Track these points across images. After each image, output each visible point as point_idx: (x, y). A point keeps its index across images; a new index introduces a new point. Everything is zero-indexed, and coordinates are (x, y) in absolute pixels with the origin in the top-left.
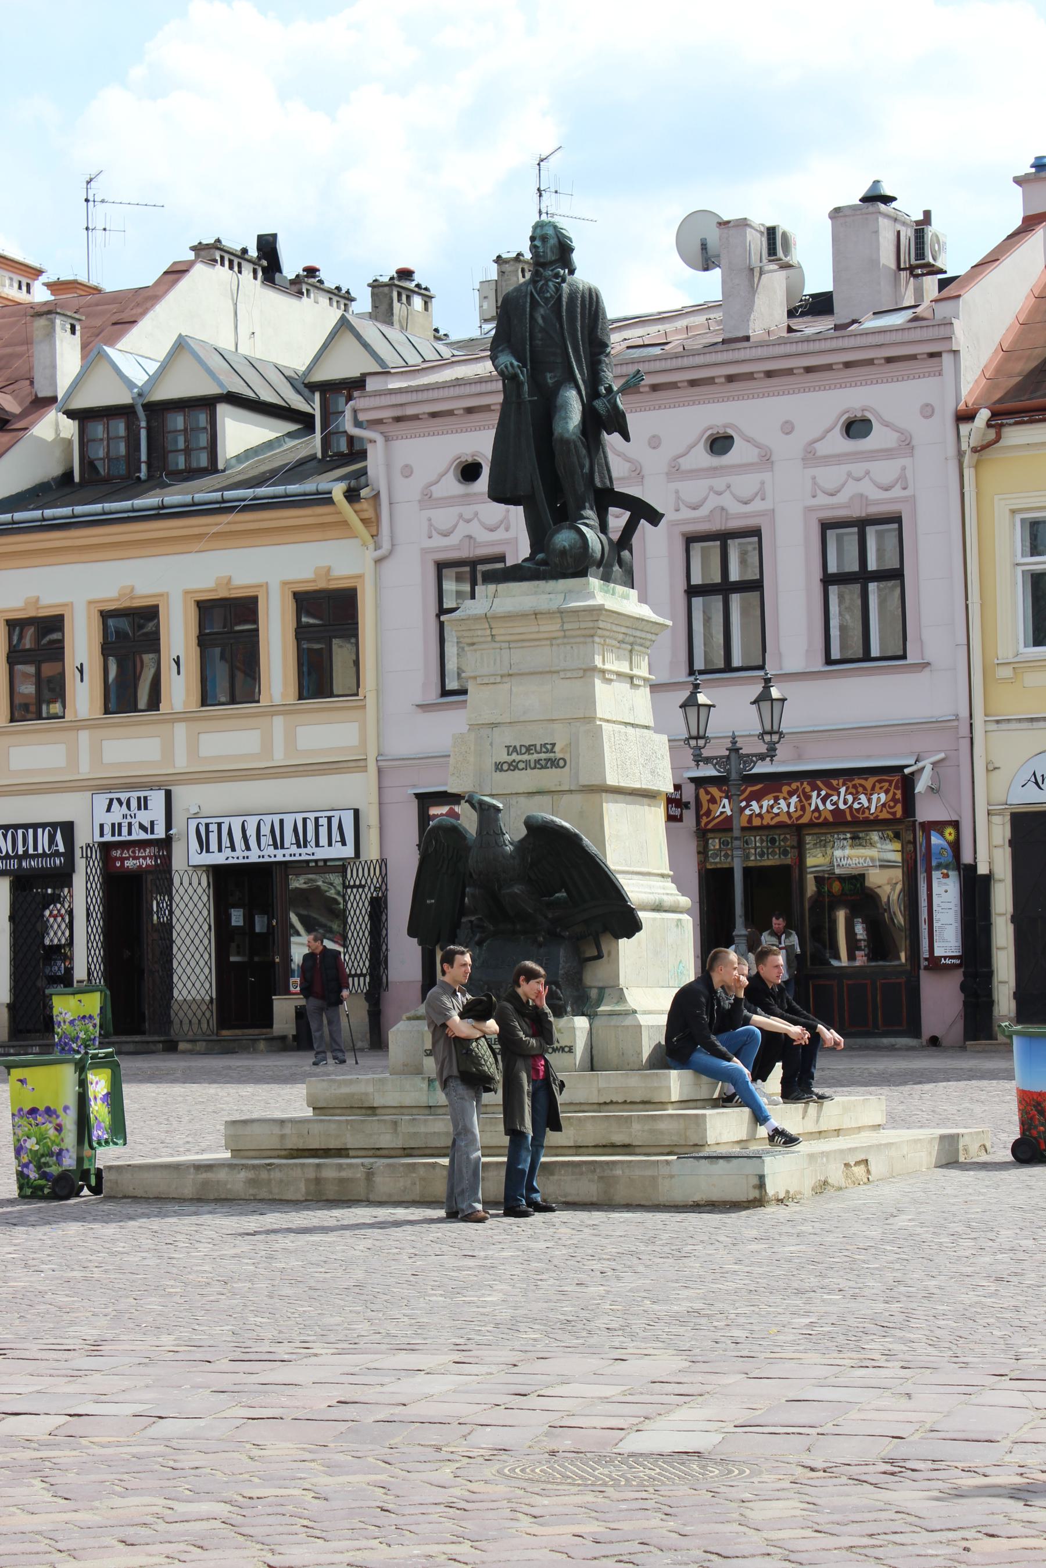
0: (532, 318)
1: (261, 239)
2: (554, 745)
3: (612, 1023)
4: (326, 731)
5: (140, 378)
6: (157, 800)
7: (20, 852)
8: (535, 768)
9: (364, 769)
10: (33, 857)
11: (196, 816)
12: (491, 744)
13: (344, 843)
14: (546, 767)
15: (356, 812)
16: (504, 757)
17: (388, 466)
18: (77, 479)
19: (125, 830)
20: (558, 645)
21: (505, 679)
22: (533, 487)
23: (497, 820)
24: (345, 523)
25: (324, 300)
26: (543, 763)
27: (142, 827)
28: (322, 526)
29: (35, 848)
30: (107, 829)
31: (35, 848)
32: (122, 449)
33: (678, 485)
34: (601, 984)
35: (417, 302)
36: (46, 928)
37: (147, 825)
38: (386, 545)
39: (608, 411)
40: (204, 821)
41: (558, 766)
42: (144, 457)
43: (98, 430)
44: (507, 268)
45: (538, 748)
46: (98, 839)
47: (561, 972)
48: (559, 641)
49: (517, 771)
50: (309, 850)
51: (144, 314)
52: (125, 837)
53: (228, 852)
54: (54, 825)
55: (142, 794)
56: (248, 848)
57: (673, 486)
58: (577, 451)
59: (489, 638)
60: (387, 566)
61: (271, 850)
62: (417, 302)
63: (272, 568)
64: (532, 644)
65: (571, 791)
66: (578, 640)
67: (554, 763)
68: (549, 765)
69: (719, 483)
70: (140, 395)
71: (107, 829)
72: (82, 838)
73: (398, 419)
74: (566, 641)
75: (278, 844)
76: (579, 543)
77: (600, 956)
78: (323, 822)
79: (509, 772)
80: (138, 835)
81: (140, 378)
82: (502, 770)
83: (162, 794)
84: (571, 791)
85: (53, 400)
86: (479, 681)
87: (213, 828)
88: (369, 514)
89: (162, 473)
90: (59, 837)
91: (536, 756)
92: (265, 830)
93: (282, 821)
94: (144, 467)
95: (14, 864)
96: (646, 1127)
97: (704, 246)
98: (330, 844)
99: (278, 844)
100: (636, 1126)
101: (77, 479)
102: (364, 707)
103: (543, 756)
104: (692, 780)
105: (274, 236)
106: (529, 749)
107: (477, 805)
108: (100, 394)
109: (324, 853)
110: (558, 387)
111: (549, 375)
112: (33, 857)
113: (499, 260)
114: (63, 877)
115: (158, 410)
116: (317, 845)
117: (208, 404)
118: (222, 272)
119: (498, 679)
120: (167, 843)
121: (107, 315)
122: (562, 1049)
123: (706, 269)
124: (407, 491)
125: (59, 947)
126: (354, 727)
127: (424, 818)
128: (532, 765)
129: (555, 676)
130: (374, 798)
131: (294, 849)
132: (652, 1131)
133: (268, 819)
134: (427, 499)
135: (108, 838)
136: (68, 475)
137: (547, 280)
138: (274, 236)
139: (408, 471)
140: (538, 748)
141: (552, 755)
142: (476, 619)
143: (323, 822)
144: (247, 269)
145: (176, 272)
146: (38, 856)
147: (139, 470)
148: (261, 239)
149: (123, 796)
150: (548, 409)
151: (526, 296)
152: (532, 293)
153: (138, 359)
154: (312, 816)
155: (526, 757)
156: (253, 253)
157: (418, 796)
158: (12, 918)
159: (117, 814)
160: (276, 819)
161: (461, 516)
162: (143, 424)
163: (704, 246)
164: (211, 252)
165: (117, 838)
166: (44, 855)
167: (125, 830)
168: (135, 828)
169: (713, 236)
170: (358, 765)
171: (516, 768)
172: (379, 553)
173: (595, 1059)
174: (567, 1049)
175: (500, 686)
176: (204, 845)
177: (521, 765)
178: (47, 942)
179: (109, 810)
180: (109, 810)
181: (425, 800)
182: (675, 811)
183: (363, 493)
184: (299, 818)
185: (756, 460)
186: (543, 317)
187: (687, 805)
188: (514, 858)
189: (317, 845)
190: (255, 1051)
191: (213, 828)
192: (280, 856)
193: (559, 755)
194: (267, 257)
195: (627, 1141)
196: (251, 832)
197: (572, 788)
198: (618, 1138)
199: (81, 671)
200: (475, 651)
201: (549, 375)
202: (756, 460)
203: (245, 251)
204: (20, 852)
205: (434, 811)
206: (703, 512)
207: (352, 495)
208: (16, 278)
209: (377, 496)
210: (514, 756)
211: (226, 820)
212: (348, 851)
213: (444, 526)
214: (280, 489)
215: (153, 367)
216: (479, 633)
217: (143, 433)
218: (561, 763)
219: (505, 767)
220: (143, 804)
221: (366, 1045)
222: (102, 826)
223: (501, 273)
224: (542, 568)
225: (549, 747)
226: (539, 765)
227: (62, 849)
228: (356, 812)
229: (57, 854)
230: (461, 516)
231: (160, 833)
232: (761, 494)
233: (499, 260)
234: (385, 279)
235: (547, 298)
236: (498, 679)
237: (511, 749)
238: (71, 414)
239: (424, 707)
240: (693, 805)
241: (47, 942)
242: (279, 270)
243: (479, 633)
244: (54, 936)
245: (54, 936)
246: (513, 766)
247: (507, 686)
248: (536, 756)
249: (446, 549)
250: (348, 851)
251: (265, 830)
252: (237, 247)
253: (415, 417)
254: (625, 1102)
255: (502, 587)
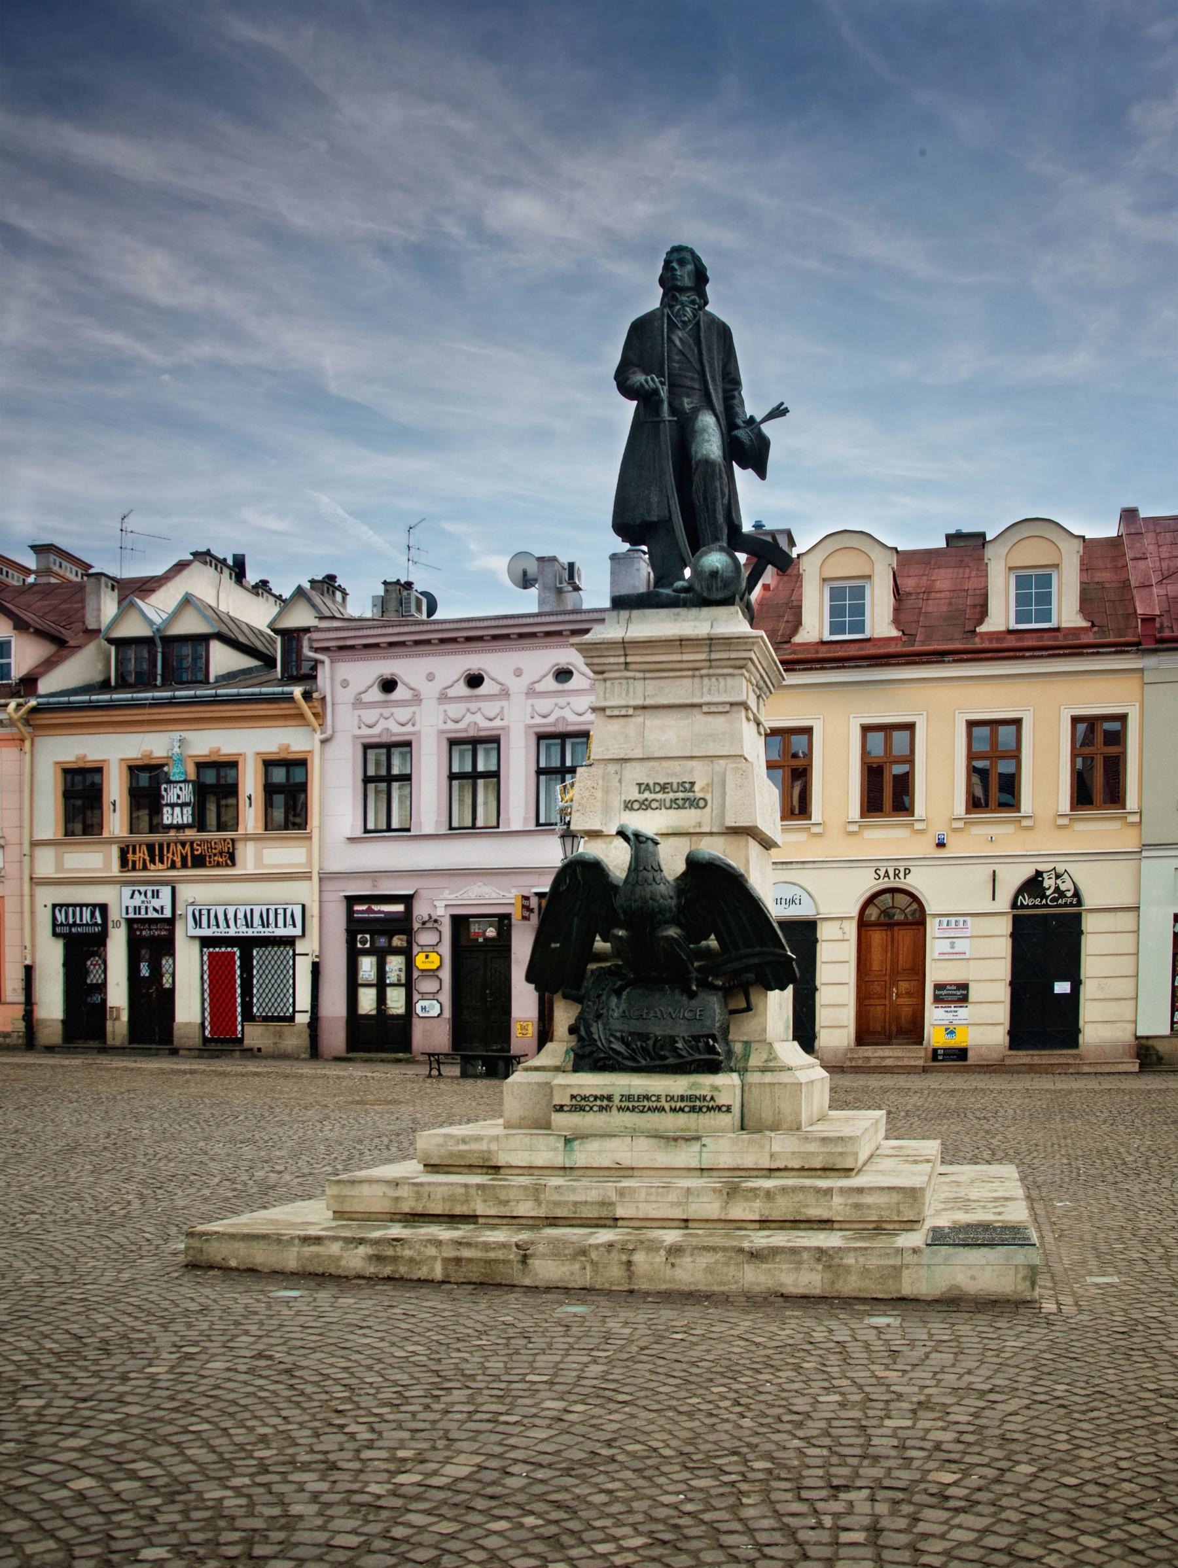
0: (670, 340)
1: (235, 556)
2: (692, 784)
3: (767, 1081)
4: (284, 854)
5: (158, 620)
6: (166, 892)
7: (71, 921)
8: (671, 808)
9: (310, 878)
10: (79, 925)
11: (192, 904)
12: (620, 781)
13: (294, 925)
14: (684, 808)
15: (304, 906)
16: (634, 794)
17: (332, 679)
18: (113, 683)
19: (143, 911)
20: (702, 676)
21: (638, 712)
22: (669, 511)
23: (655, 854)
24: (301, 716)
25: (272, 599)
26: (680, 802)
27: (155, 909)
28: (285, 717)
29: (81, 919)
30: (131, 910)
31: (81, 919)
32: (145, 666)
33: (533, 701)
34: (745, 1039)
35: (339, 595)
36: (87, 973)
37: (158, 908)
38: (329, 732)
39: (751, 440)
40: (198, 908)
41: (698, 807)
42: (159, 671)
43: (131, 654)
44: (390, 588)
45: (675, 786)
46: (124, 915)
47: (717, 1025)
48: (703, 672)
49: (649, 811)
50: (270, 929)
51: (160, 586)
52: (143, 915)
53: (214, 929)
54: (94, 906)
55: (155, 888)
56: (228, 926)
57: (530, 702)
58: (721, 477)
59: (622, 667)
60: (328, 746)
61: (244, 929)
62: (339, 595)
63: (249, 744)
64: (671, 674)
65: (711, 834)
66: (726, 671)
67: (694, 803)
68: (687, 805)
69: (562, 701)
70: (158, 630)
71: (131, 910)
72: (114, 914)
73: (341, 648)
74: (711, 671)
75: (249, 924)
76: (731, 567)
77: (749, 1009)
78: (281, 911)
79: (641, 811)
80: (152, 915)
81: (158, 621)
82: (632, 809)
83: (169, 889)
84: (711, 834)
85: (99, 631)
86: (608, 712)
87: (205, 912)
88: (319, 710)
89: (172, 677)
90: (97, 914)
91: (672, 795)
92: (240, 915)
93: (252, 910)
94: (159, 678)
95: (66, 930)
96: (850, 1201)
97: (525, 573)
98: (285, 926)
99: (249, 924)
100: (837, 1200)
101: (113, 683)
102: (311, 838)
103: (680, 795)
104: (537, 894)
105: (244, 556)
106: (664, 788)
107: (631, 837)
108: (133, 628)
109: (281, 932)
110: (696, 411)
111: (686, 400)
112: (79, 925)
113: (385, 583)
114: (99, 940)
115: (171, 641)
116: (276, 926)
117: (204, 639)
118: (210, 571)
119: (631, 712)
120: (171, 922)
121: (134, 590)
122: (719, 1108)
123: (525, 588)
124: (345, 696)
125: (97, 985)
126: (304, 850)
127: (350, 912)
128: (668, 805)
129: (696, 710)
130: (316, 897)
131: (260, 928)
132: (857, 1206)
133: (242, 908)
134: (358, 703)
135: (131, 915)
136: (108, 680)
137: (683, 305)
138: (244, 556)
139: (345, 684)
140: (675, 786)
141: (691, 794)
142: (610, 644)
143: (281, 911)
144: (226, 572)
145: (181, 566)
146: (83, 925)
147: (156, 680)
148: (235, 556)
149: (142, 889)
150: (685, 432)
151: (662, 319)
152: (668, 316)
153: (158, 608)
154: (273, 907)
155: (660, 796)
156: (230, 562)
157: (347, 897)
158: (65, 965)
159: (138, 900)
160: (248, 908)
161: (381, 715)
162: (160, 650)
163: (525, 573)
164: (204, 557)
165: (137, 916)
166: (87, 925)
167: (143, 911)
168: (150, 910)
169: (533, 568)
170: (306, 876)
171: (648, 807)
172: (323, 736)
173: (746, 1119)
174: (724, 1109)
175: (633, 719)
176: (198, 923)
177: (654, 805)
178: (89, 981)
179: (132, 897)
180: (132, 897)
181: (351, 900)
182: (526, 914)
183: (315, 695)
184: (264, 908)
185: (587, 687)
186: (681, 339)
187: (531, 911)
188: (671, 898)
189: (276, 926)
190: (233, 1057)
191: (205, 912)
192: (250, 933)
193: (699, 795)
194: (238, 569)
195: (826, 1215)
196: (231, 916)
197: (714, 830)
198: (814, 1212)
199: (114, 805)
200: (605, 680)
201: (686, 400)
202: (587, 687)
203: (225, 560)
204: (71, 921)
205: (357, 908)
206: (551, 719)
207: (307, 696)
208: (75, 569)
209: (323, 699)
210: (647, 795)
211: (214, 908)
212: (297, 931)
213: (369, 722)
214: (256, 690)
215: (165, 616)
216: (612, 660)
217: (159, 656)
218: (702, 803)
219: (636, 806)
220: (156, 895)
221: (306, 1056)
222: (127, 908)
223: (386, 591)
224: (682, 595)
225: (687, 785)
226: (675, 805)
227: (99, 921)
228: (304, 906)
229: (96, 924)
230: (381, 715)
231: (168, 913)
232: (500, 715)
233: (385, 583)
234: (320, 578)
235: (684, 322)
236: (631, 712)
237: (643, 787)
238: (111, 641)
239: (352, 840)
240: (536, 911)
241: (89, 981)
242: (244, 576)
243: (612, 660)
244: (94, 978)
245: (94, 978)
246: (645, 805)
247: (640, 720)
248: (672, 795)
249: (371, 736)
250: (297, 931)
251: (240, 915)
252: (221, 557)
253: (352, 647)
254: (802, 1169)
255: (635, 613)
